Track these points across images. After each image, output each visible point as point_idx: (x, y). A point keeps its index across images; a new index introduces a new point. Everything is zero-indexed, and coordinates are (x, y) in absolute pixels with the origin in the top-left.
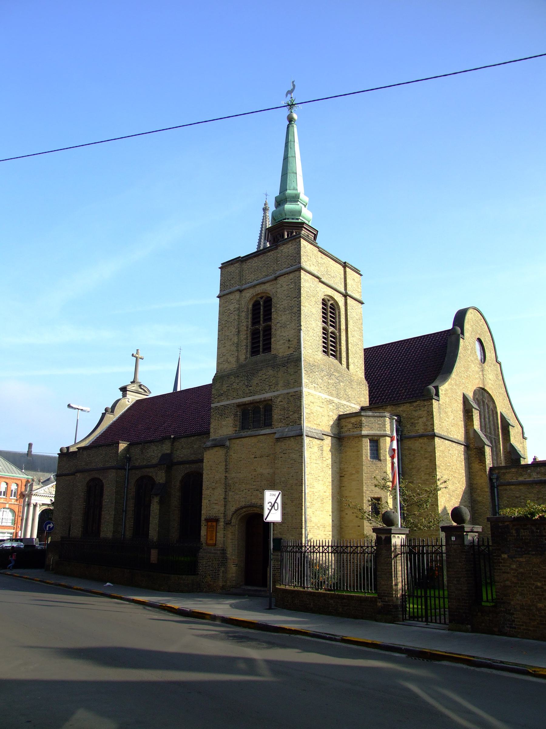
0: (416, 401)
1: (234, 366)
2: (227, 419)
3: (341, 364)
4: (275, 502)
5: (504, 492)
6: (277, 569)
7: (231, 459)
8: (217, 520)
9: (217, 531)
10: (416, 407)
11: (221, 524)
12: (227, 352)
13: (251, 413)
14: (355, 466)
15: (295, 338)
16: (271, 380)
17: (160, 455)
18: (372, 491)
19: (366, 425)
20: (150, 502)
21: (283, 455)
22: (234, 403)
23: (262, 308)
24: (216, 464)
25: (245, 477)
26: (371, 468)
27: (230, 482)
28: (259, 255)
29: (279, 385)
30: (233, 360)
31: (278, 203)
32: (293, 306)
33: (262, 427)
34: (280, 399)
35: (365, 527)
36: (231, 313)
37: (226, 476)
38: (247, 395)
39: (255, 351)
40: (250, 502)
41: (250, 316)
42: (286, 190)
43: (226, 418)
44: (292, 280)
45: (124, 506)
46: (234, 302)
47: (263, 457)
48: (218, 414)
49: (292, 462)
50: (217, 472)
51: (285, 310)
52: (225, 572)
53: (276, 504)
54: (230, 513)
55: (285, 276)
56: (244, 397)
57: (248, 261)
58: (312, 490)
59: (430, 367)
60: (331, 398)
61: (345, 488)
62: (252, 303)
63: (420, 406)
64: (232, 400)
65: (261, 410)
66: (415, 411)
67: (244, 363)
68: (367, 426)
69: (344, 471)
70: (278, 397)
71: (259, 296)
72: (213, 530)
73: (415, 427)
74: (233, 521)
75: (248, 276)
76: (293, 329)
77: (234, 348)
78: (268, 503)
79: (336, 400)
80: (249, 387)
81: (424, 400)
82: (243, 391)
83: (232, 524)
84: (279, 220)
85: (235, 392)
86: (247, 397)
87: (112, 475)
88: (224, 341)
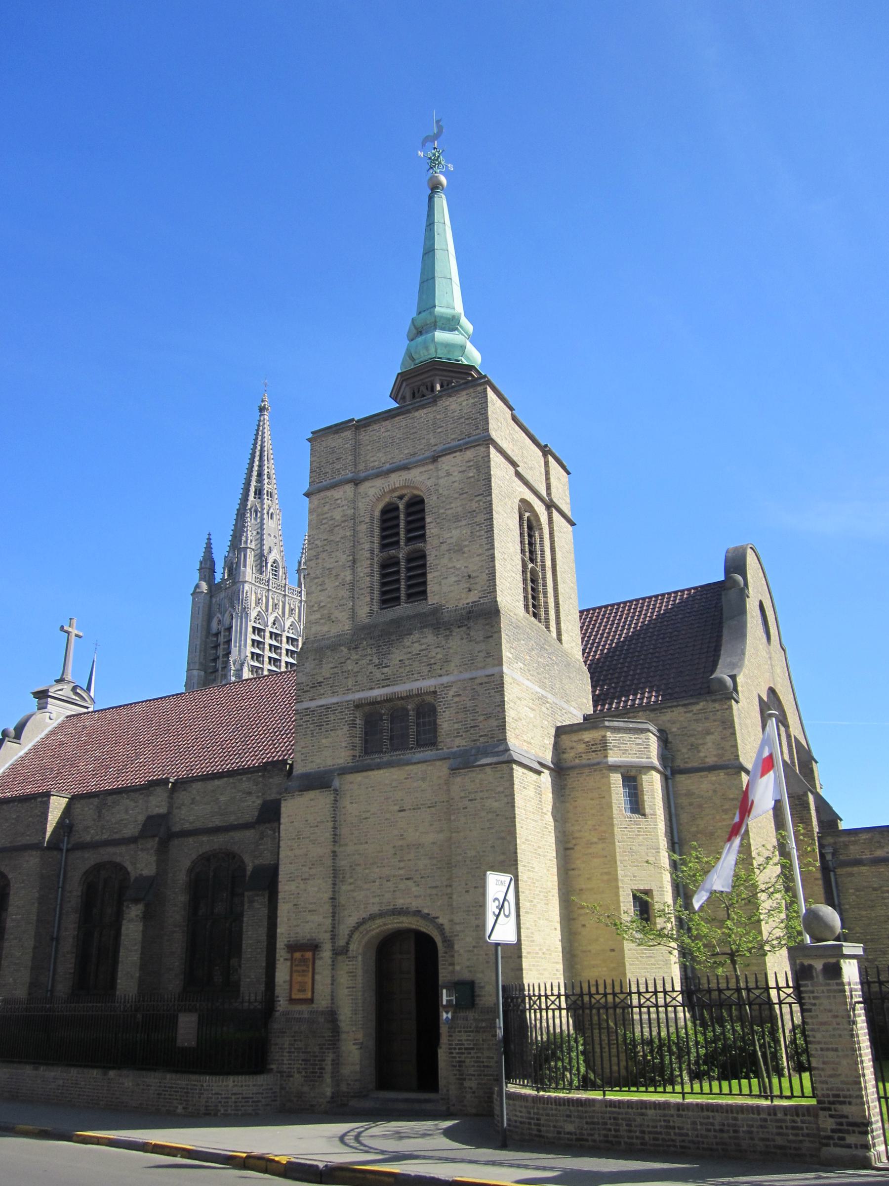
0: (697, 703)
1: (346, 628)
2: (332, 733)
3: (549, 631)
4: (505, 899)
5: (849, 879)
6: (466, 1049)
7: (345, 814)
8: (314, 947)
9: (317, 971)
10: (699, 714)
11: (326, 954)
12: (329, 600)
13: (387, 720)
14: (597, 827)
15: (481, 572)
16: (434, 654)
17: (141, 818)
18: (634, 877)
19: (615, 746)
20: (119, 916)
21: (467, 803)
22: (349, 701)
23: (402, 516)
24: (311, 827)
25: (379, 852)
26: (629, 831)
27: (343, 863)
28: (395, 417)
29: (453, 664)
30: (343, 616)
31: (416, 328)
32: (474, 511)
33: (412, 748)
34: (456, 690)
35: (626, 952)
36: (337, 526)
37: (334, 852)
38: (381, 685)
39: (389, 598)
40: (392, 904)
41: (377, 532)
42: (435, 306)
43: (331, 730)
44: (471, 463)
45: (54, 927)
46: (344, 503)
47: (420, 808)
48: (311, 724)
49: (490, 816)
50: (314, 844)
51: (457, 518)
52: (336, 1064)
53: (506, 904)
54: (344, 931)
55: (454, 455)
56: (371, 689)
57: (371, 427)
58: (531, 874)
59: (687, 646)
60: (543, 692)
61: (576, 872)
62: (380, 506)
63: (706, 712)
64: (344, 694)
65: (411, 713)
66: (697, 721)
67: (367, 621)
68: (616, 749)
69: (573, 838)
70: (450, 686)
71: (397, 494)
72: (305, 968)
73: (699, 752)
74: (352, 947)
75: (370, 455)
76: (478, 555)
77: (344, 593)
78: (494, 901)
79: (551, 698)
80: (383, 667)
81: (714, 701)
82: (368, 676)
83: (350, 954)
84: (421, 360)
85: (350, 679)
86: (379, 687)
87: (31, 862)
88: (321, 579)
